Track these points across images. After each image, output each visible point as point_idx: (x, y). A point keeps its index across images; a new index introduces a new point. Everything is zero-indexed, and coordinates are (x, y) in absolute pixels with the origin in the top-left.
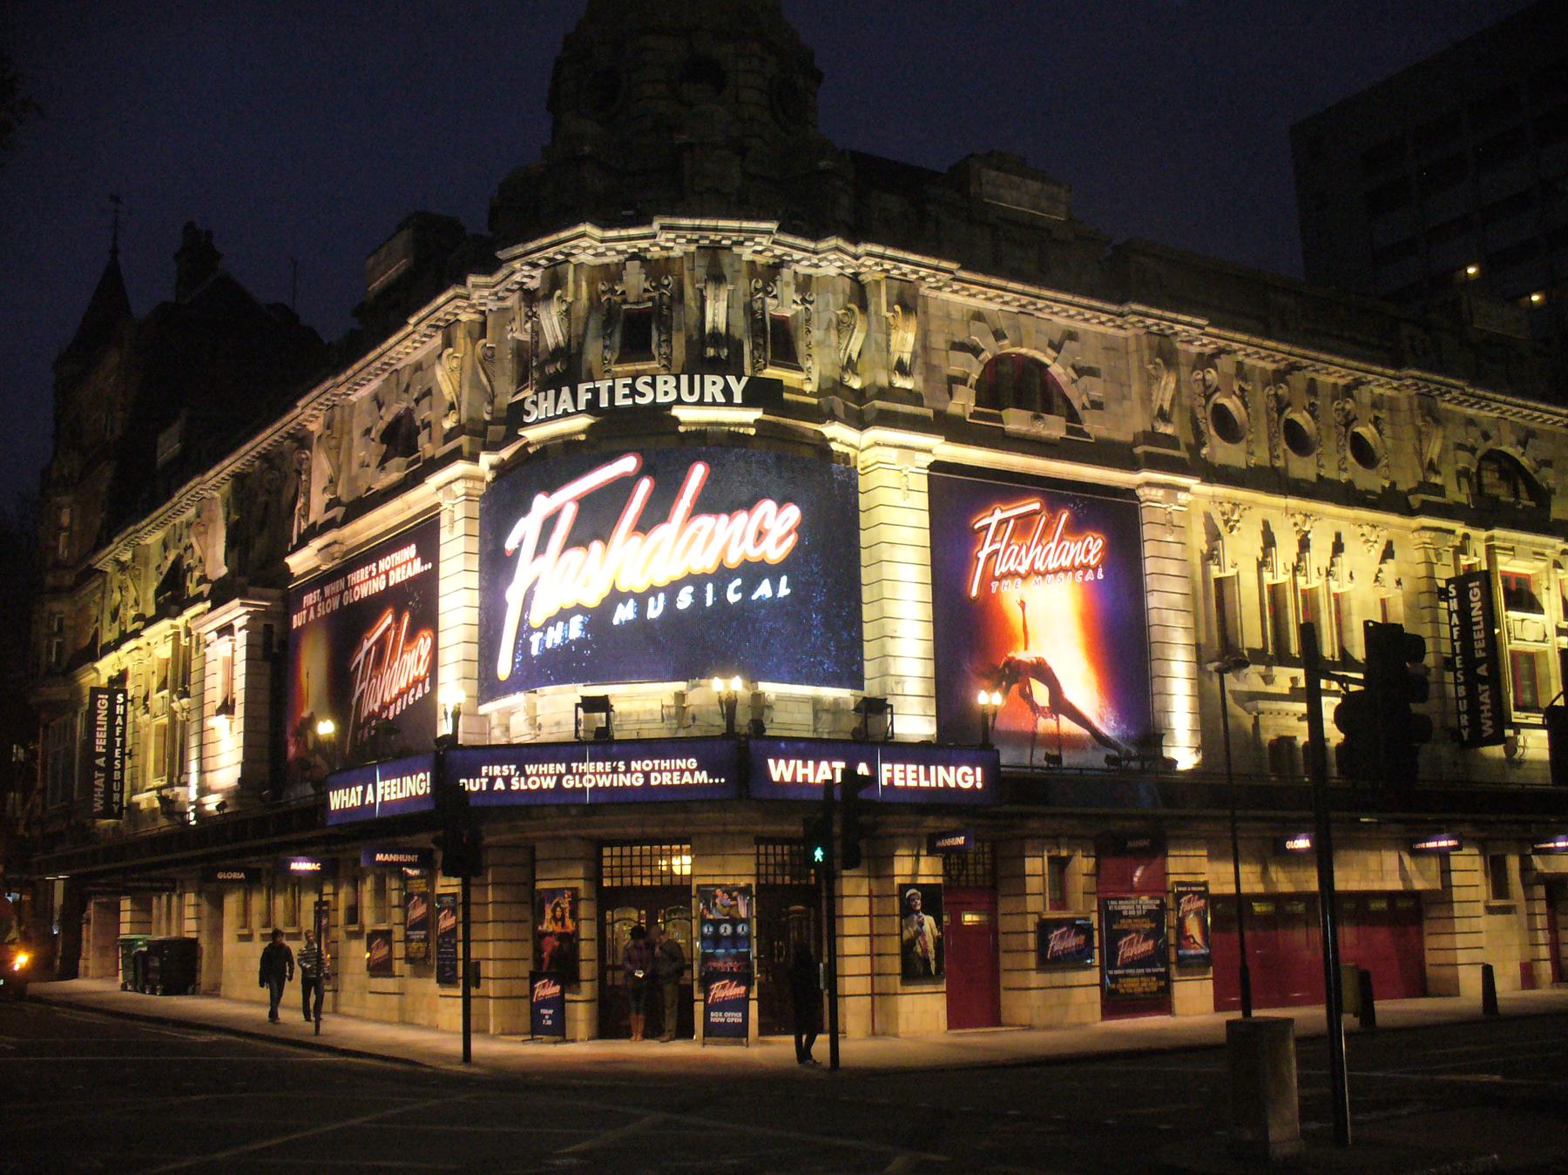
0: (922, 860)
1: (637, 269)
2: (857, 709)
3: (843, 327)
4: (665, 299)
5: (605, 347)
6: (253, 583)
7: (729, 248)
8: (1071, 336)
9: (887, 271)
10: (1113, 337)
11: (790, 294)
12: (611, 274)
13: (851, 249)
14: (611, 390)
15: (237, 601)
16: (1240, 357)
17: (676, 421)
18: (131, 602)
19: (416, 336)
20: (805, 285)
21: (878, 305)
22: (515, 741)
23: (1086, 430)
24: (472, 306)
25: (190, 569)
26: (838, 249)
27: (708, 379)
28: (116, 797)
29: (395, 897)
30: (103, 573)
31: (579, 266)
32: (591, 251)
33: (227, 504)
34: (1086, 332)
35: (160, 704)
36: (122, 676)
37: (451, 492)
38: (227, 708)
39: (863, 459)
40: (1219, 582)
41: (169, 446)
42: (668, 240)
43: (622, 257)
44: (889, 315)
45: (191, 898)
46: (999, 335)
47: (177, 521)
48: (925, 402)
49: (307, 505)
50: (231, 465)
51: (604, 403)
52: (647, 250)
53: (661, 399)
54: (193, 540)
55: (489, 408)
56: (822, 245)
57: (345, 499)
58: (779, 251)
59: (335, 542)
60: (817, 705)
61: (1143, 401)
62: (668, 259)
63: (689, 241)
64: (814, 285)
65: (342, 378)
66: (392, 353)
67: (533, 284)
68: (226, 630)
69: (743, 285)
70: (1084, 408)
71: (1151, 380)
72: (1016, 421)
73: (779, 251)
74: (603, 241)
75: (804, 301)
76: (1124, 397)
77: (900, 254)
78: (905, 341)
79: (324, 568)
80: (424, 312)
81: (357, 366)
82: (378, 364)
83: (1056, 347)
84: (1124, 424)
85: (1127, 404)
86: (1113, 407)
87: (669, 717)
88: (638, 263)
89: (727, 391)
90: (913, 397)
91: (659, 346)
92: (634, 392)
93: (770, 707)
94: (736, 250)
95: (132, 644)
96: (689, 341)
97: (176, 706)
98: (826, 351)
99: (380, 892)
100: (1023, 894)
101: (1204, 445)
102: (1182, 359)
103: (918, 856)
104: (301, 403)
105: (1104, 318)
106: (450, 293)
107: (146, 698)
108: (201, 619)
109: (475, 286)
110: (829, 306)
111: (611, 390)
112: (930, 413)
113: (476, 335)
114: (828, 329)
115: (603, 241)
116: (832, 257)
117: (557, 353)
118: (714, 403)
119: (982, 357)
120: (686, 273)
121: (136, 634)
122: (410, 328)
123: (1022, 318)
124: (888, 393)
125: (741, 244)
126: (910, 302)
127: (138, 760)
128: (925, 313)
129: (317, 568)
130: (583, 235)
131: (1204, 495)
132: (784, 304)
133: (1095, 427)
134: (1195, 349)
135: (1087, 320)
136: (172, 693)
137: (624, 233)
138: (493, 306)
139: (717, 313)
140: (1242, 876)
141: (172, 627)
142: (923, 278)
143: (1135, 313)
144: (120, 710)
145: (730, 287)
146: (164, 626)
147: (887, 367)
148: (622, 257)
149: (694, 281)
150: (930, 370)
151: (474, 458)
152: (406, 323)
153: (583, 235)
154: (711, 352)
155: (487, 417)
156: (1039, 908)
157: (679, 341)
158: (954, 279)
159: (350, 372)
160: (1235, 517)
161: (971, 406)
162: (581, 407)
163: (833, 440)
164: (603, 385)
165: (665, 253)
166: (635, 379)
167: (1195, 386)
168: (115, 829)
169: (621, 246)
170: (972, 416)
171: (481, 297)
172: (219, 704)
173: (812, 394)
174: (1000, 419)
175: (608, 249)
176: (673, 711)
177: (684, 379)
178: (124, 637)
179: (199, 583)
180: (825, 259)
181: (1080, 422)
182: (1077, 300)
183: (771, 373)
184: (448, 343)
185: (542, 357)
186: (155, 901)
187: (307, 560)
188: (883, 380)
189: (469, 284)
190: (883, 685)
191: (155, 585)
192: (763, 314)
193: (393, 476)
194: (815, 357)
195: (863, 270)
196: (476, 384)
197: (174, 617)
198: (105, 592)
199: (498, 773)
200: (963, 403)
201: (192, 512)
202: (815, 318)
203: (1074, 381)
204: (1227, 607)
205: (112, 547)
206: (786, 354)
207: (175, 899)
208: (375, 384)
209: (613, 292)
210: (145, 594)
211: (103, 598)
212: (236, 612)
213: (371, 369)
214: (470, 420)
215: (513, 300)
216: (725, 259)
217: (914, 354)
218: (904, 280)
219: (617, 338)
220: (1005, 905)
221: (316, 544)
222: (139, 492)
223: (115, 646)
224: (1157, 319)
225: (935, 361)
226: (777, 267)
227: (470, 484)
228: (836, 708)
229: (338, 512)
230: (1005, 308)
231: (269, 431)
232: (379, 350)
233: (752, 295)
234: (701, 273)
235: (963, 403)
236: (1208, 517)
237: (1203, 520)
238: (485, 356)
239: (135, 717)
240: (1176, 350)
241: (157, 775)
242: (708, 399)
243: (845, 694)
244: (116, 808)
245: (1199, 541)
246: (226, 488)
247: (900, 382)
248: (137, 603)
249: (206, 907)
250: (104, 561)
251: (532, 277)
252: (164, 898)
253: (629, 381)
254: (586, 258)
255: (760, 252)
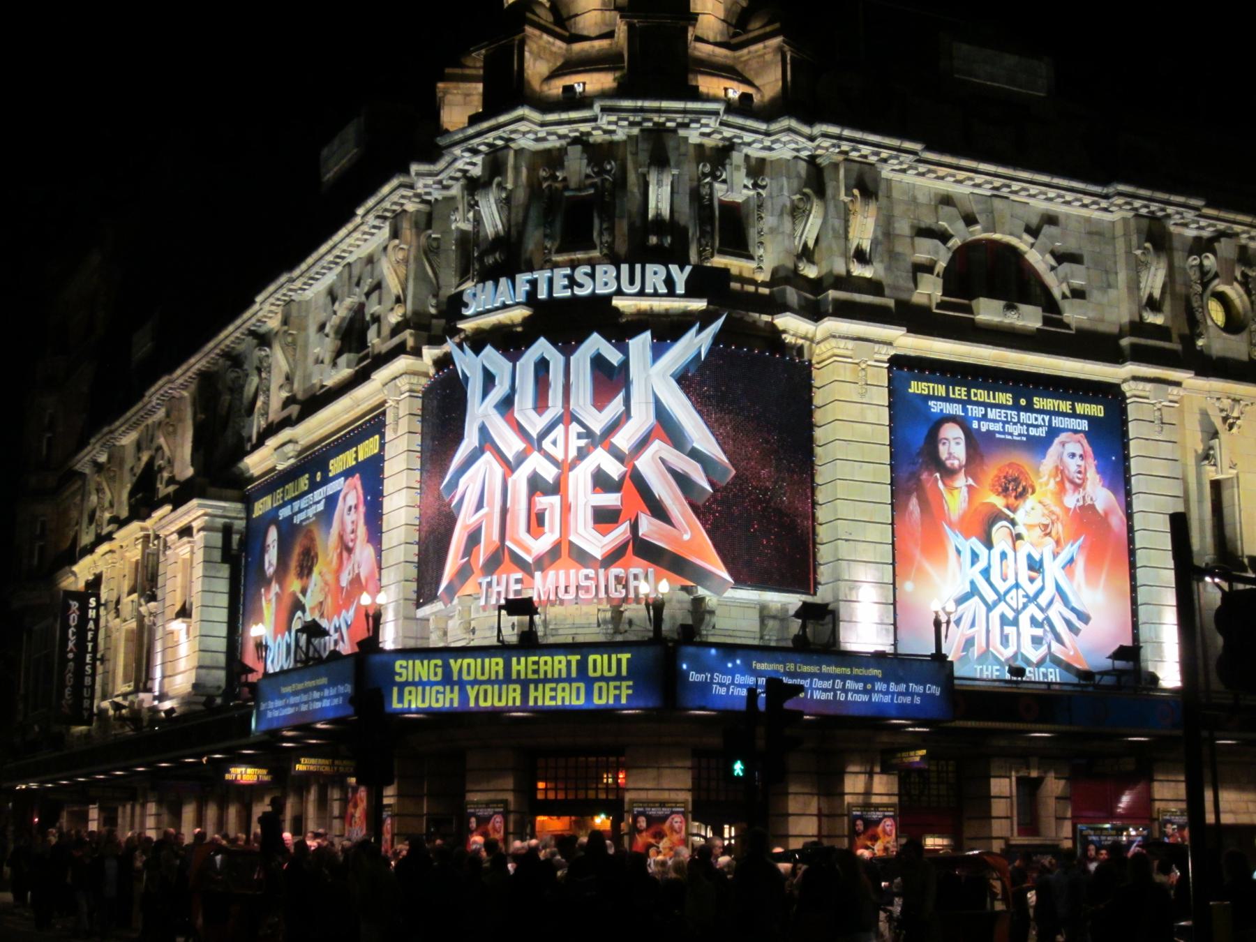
0: (877, 779)
1: (579, 155)
2: (798, 614)
3: (797, 213)
4: (607, 185)
5: (546, 236)
6: (213, 484)
7: (674, 131)
8: (1051, 220)
9: (846, 153)
10: (1099, 222)
11: (741, 178)
12: (553, 159)
13: (806, 130)
14: (551, 281)
15: (195, 502)
16: (1243, 239)
17: (616, 310)
18: (107, 504)
19: (365, 228)
20: (757, 169)
21: (837, 188)
22: (453, 645)
23: (1066, 320)
24: (418, 195)
25: (161, 469)
26: (790, 130)
27: (650, 268)
28: (86, 703)
29: (336, 809)
30: (82, 476)
31: (519, 152)
32: (531, 136)
33: (194, 404)
34: (1068, 216)
35: (129, 607)
36: (95, 584)
37: (397, 385)
38: (184, 613)
39: (820, 352)
40: (1216, 486)
41: (142, 346)
42: (610, 123)
43: (564, 142)
44: (847, 199)
45: (152, 808)
46: (970, 220)
47: (150, 421)
48: (887, 292)
49: (266, 404)
50: (197, 363)
51: (542, 295)
52: (589, 134)
53: (601, 291)
54: (162, 441)
55: (434, 302)
56: (774, 127)
57: (300, 396)
58: (728, 132)
59: (290, 441)
60: (764, 614)
61: (1130, 289)
62: (612, 143)
63: (632, 124)
64: (768, 169)
65: (297, 272)
66: (343, 246)
67: (476, 171)
68: (186, 532)
69: (690, 170)
70: (1064, 297)
71: (1137, 267)
72: (988, 311)
73: (728, 132)
74: (543, 125)
75: (755, 186)
76: (1109, 286)
77: (858, 135)
78: (863, 229)
79: (280, 467)
80: (371, 202)
81: (310, 260)
82: (330, 258)
83: (1033, 232)
84: (1110, 310)
85: (1113, 293)
86: (1096, 295)
87: (605, 622)
88: (579, 148)
89: (669, 282)
90: (874, 287)
91: (601, 234)
92: (573, 282)
93: (712, 612)
94: (682, 132)
95: (104, 547)
96: (631, 227)
97: (143, 609)
98: (780, 237)
99: (323, 803)
100: (987, 816)
101: (1200, 336)
102: (1176, 244)
103: (871, 774)
104: (259, 299)
105: (1087, 200)
106: (395, 182)
107: (118, 602)
108: (165, 520)
109: (419, 174)
110: (782, 191)
111: (551, 281)
112: (891, 303)
113: (422, 225)
114: (781, 214)
115: (543, 125)
116: (785, 138)
117: (499, 242)
118: (655, 294)
119: (950, 244)
120: (629, 157)
121: (109, 537)
122: (358, 220)
123: (997, 203)
124: (845, 282)
125: (686, 126)
126: (870, 186)
127: (110, 665)
128: (889, 197)
129: (274, 469)
130: (521, 119)
131: (1199, 391)
132: (734, 188)
133: (1075, 315)
134: (1191, 233)
135: (1068, 203)
136: (140, 596)
137: (564, 116)
138: (437, 194)
139: (660, 199)
140: (1222, 805)
141: (143, 529)
142: (885, 161)
143: (1120, 194)
144: (92, 613)
145: (675, 172)
146: (135, 525)
147: (845, 254)
148: (564, 142)
149: (637, 165)
150: (893, 257)
151: (417, 353)
152: (354, 215)
153: (521, 119)
154: (653, 240)
155: (433, 311)
156: (1006, 834)
157: (623, 227)
158: (920, 161)
159: (304, 266)
160: (1235, 414)
161: (938, 295)
162: (521, 298)
163: (784, 332)
164: (542, 276)
165: (607, 137)
166: (573, 268)
167: (1191, 273)
168: (88, 735)
169: (563, 130)
170: (939, 306)
171: (426, 186)
172: (178, 607)
173: (764, 284)
174: (969, 309)
175: (549, 134)
176: (609, 615)
177: (625, 268)
178: (100, 539)
179: (168, 484)
180: (777, 141)
181: (1059, 312)
182: (1056, 181)
183: (719, 261)
184: (395, 234)
185: (483, 247)
186: (120, 810)
187: (264, 460)
188: (839, 268)
189: (413, 173)
190: (836, 591)
191: (129, 486)
192: (711, 199)
193: (344, 372)
194: (769, 246)
195: (819, 152)
196: (421, 277)
197: (143, 519)
198: (85, 496)
199: (806, 790)
200: (929, 291)
201: (161, 413)
202: (768, 204)
203: (1053, 268)
204: (1226, 511)
205: (89, 448)
206: (738, 244)
207: (138, 809)
208: (330, 278)
209: (555, 178)
210: (120, 496)
211: (82, 500)
212: (195, 512)
213: (324, 262)
214: (415, 313)
215: (456, 190)
216: (671, 144)
217: (875, 242)
218: (864, 163)
219: (558, 225)
220: (969, 830)
221: (272, 443)
222: (116, 395)
223: (90, 550)
224: (1147, 202)
225: (899, 248)
226: (728, 148)
227: (415, 380)
228: (781, 617)
229: (294, 410)
230: (977, 191)
231: (231, 328)
232: (330, 243)
233: (699, 180)
234: (644, 157)
235: (929, 291)
236: (1204, 414)
237: (1198, 417)
238: (430, 246)
239: (107, 621)
240: (1170, 234)
241: (126, 680)
242: (649, 290)
243: (793, 601)
244: (86, 714)
245: (1195, 442)
246: (193, 387)
247: (858, 270)
248: (112, 505)
249: (166, 818)
250: (83, 462)
251: (474, 164)
252: (128, 807)
253: (568, 271)
254: (526, 143)
255: (708, 135)
